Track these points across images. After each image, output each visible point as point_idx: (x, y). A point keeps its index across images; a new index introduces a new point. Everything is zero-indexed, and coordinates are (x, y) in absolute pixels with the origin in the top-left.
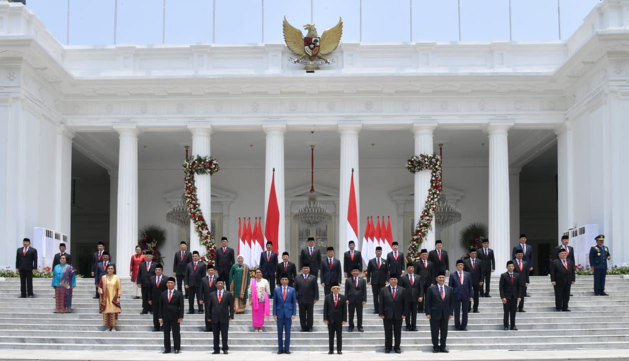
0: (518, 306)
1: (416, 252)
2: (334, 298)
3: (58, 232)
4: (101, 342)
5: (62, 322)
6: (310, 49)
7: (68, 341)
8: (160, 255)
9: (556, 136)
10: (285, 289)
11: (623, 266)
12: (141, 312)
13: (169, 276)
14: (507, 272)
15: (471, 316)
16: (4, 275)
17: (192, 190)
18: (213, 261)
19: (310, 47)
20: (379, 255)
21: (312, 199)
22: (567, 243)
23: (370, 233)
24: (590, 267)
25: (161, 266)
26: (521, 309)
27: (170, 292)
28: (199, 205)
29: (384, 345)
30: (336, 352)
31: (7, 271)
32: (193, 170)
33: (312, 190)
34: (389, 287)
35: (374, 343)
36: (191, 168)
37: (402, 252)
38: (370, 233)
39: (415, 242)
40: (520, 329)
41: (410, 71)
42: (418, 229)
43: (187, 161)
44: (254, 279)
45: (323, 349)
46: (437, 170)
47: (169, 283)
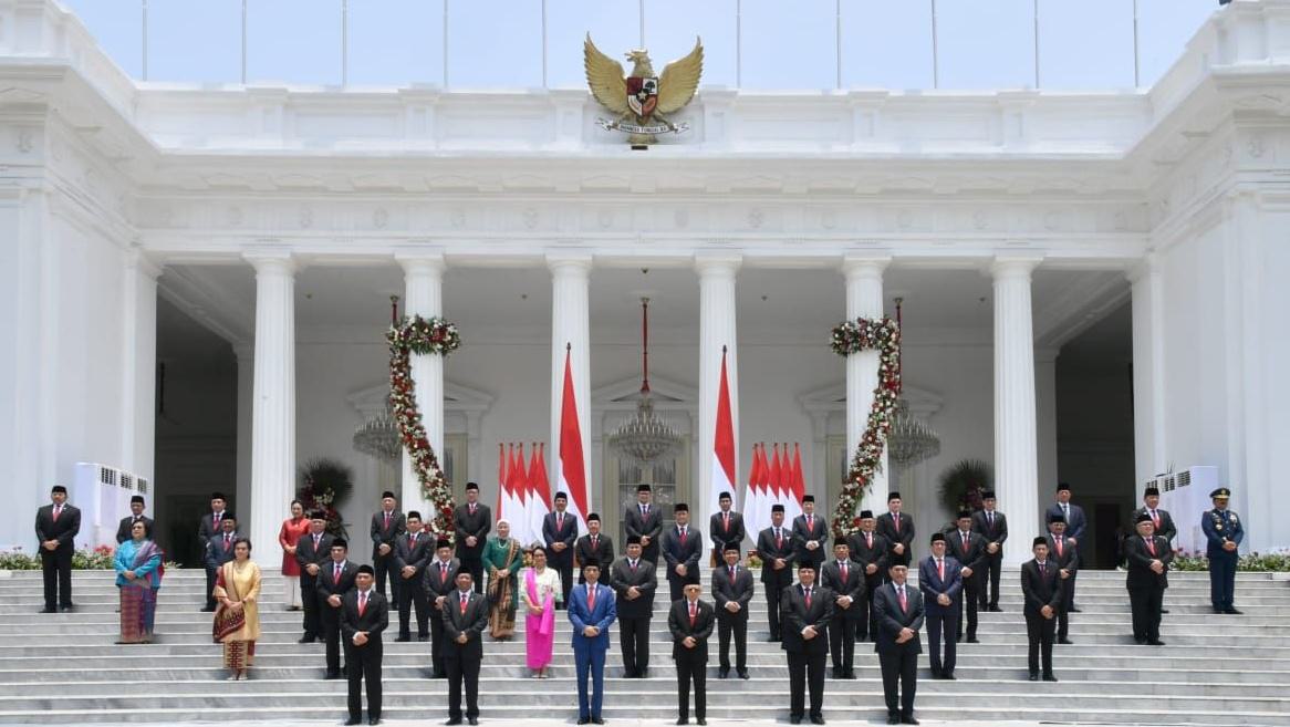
0: (1056, 632)
1: (852, 517)
2: (690, 608)
3: (129, 472)
4: (216, 703)
5: (134, 662)
6: (641, 101)
7: (146, 702)
8: (341, 519)
9: (1129, 284)
10: (592, 588)
11: (1271, 553)
12: (301, 638)
13: (360, 564)
14: (1034, 561)
15: (963, 650)
16: (8, 565)
17: (405, 385)
18: (449, 533)
19: (638, 97)
20: (778, 523)
21: (646, 408)
22: (1156, 503)
23: (760, 476)
24: (1204, 558)
25: (343, 543)
26: (1063, 639)
27: (363, 595)
28: (420, 416)
29: (789, 707)
30: (693, 720)
31: (16, 556)
32: (408, 346)
33: (645, 388)
34: (799, 586)
35: (770, 704)
36: (403, 342)
37: (823, 515)
38: (760, 476)
39: (849, 497)
40: (1062, 679)
41: (840, 149)
42: (855, 469)
43: (396, 327)
44: (530, 569)
45: (668, 713)
46: (891, 350)
47: (360, 577)
